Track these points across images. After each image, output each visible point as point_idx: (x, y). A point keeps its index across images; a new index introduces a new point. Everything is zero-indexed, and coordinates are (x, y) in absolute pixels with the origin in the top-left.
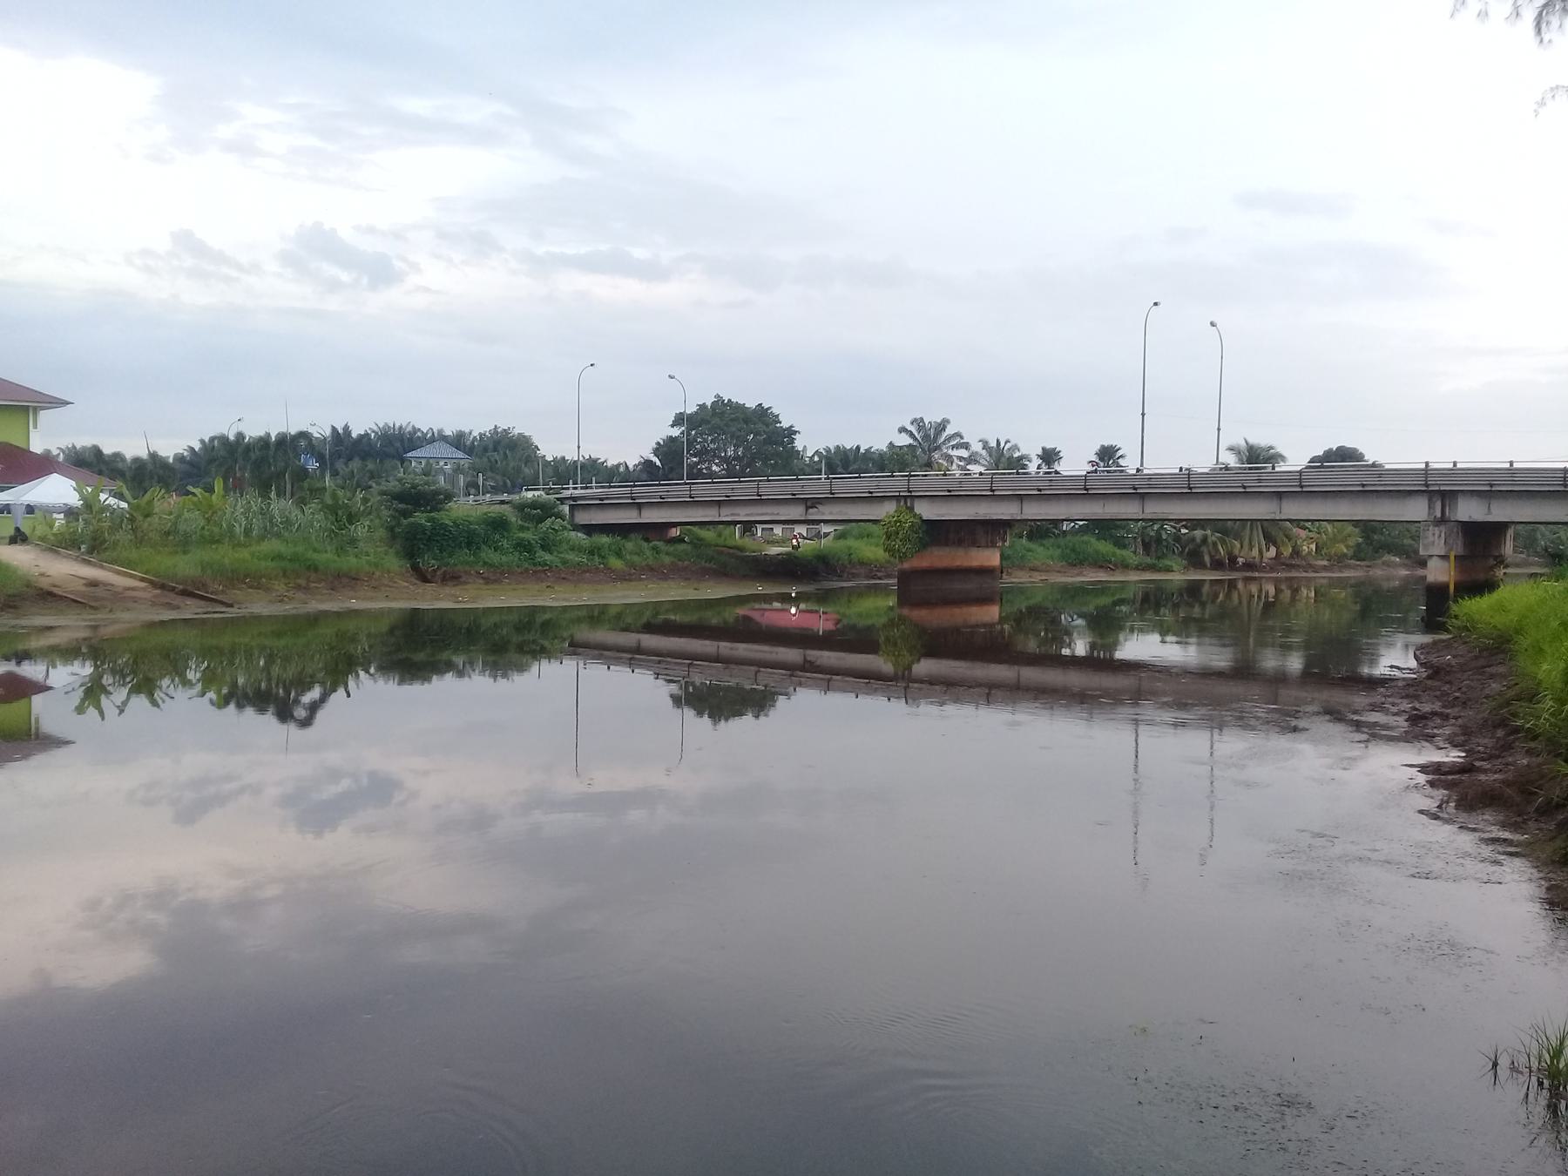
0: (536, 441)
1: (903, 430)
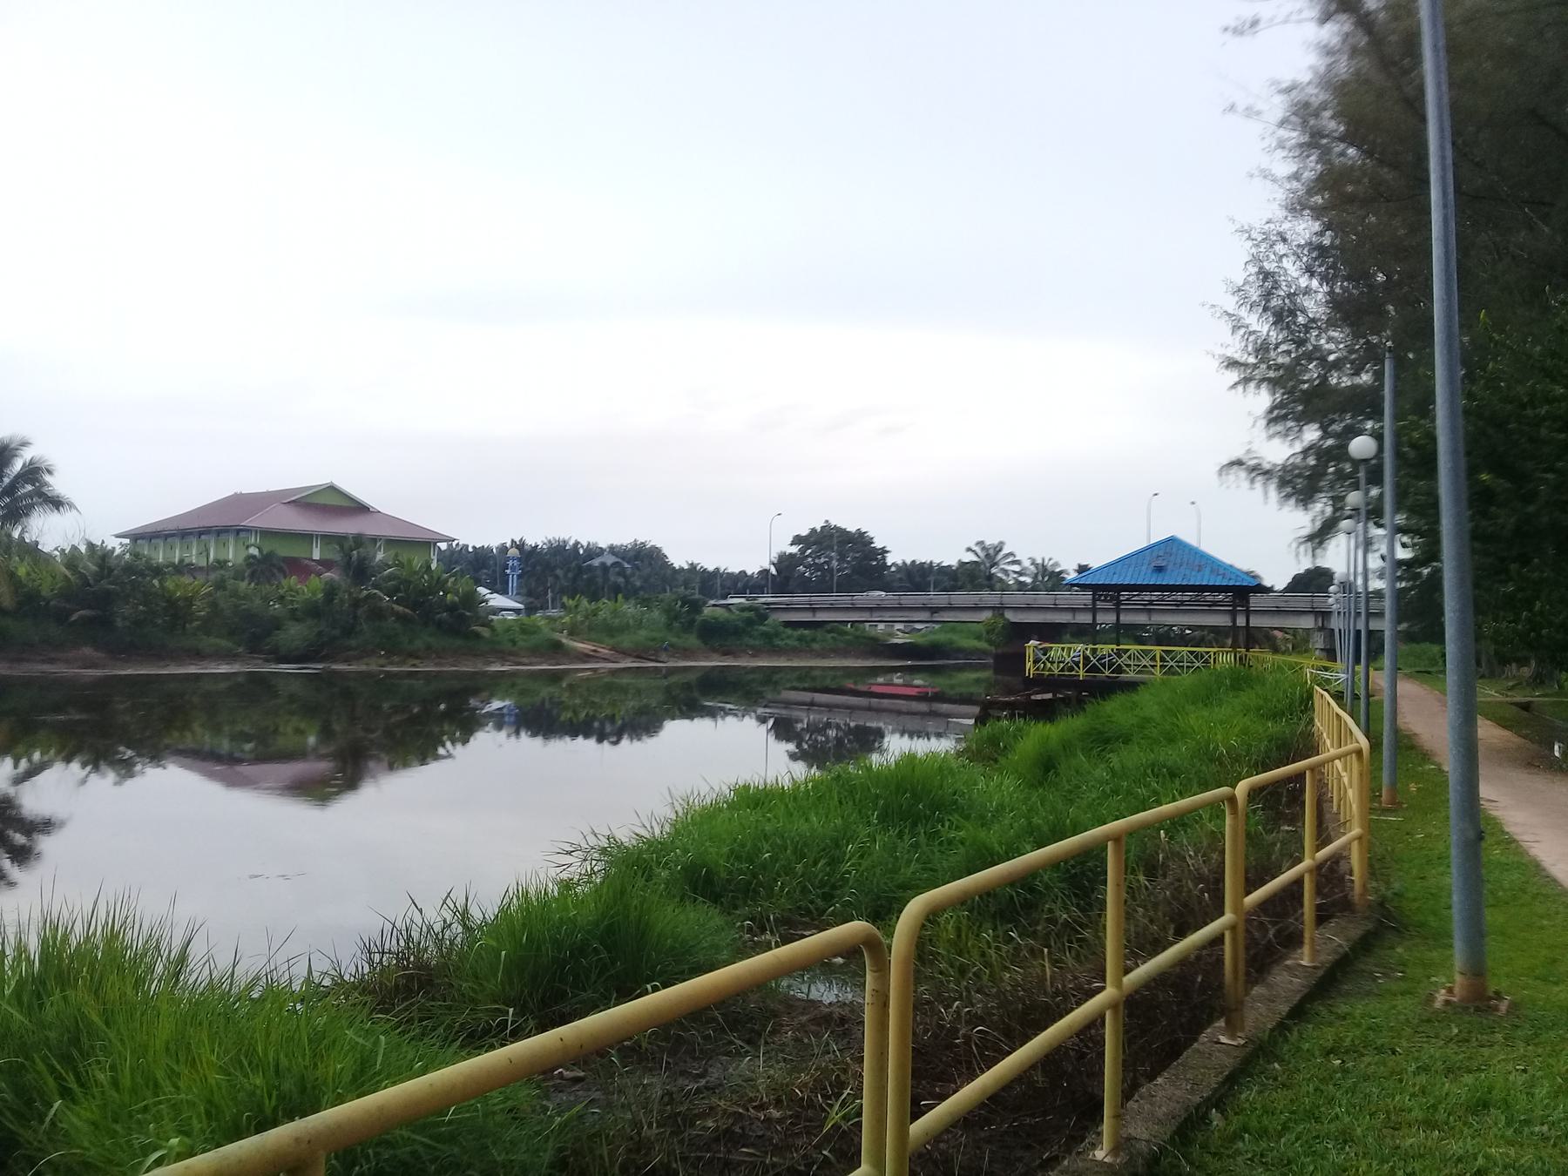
0: (665, 551)
1: (969, 549)
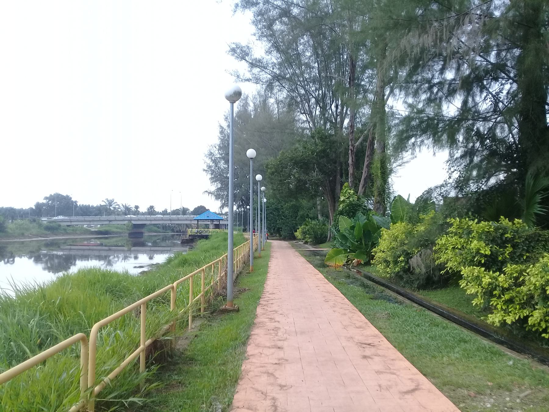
1: (103, 201)
